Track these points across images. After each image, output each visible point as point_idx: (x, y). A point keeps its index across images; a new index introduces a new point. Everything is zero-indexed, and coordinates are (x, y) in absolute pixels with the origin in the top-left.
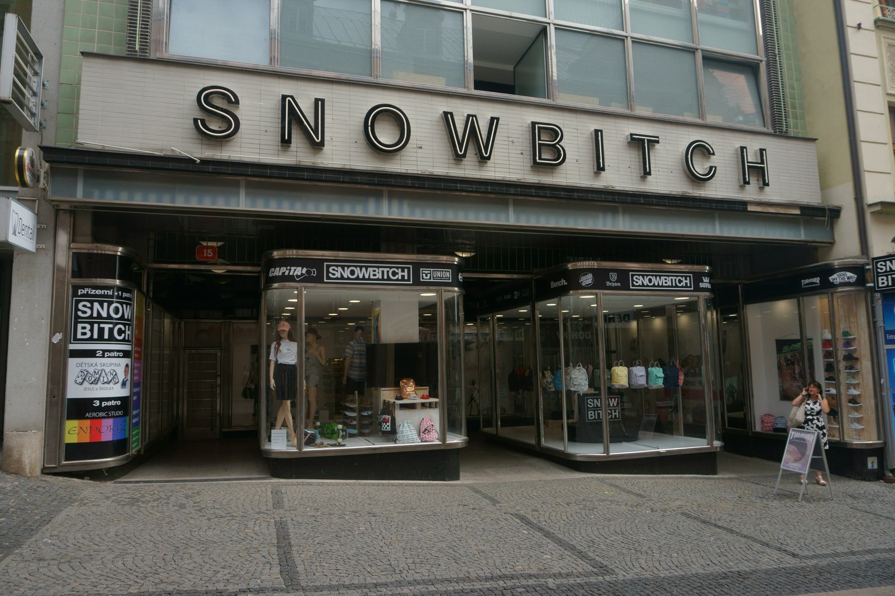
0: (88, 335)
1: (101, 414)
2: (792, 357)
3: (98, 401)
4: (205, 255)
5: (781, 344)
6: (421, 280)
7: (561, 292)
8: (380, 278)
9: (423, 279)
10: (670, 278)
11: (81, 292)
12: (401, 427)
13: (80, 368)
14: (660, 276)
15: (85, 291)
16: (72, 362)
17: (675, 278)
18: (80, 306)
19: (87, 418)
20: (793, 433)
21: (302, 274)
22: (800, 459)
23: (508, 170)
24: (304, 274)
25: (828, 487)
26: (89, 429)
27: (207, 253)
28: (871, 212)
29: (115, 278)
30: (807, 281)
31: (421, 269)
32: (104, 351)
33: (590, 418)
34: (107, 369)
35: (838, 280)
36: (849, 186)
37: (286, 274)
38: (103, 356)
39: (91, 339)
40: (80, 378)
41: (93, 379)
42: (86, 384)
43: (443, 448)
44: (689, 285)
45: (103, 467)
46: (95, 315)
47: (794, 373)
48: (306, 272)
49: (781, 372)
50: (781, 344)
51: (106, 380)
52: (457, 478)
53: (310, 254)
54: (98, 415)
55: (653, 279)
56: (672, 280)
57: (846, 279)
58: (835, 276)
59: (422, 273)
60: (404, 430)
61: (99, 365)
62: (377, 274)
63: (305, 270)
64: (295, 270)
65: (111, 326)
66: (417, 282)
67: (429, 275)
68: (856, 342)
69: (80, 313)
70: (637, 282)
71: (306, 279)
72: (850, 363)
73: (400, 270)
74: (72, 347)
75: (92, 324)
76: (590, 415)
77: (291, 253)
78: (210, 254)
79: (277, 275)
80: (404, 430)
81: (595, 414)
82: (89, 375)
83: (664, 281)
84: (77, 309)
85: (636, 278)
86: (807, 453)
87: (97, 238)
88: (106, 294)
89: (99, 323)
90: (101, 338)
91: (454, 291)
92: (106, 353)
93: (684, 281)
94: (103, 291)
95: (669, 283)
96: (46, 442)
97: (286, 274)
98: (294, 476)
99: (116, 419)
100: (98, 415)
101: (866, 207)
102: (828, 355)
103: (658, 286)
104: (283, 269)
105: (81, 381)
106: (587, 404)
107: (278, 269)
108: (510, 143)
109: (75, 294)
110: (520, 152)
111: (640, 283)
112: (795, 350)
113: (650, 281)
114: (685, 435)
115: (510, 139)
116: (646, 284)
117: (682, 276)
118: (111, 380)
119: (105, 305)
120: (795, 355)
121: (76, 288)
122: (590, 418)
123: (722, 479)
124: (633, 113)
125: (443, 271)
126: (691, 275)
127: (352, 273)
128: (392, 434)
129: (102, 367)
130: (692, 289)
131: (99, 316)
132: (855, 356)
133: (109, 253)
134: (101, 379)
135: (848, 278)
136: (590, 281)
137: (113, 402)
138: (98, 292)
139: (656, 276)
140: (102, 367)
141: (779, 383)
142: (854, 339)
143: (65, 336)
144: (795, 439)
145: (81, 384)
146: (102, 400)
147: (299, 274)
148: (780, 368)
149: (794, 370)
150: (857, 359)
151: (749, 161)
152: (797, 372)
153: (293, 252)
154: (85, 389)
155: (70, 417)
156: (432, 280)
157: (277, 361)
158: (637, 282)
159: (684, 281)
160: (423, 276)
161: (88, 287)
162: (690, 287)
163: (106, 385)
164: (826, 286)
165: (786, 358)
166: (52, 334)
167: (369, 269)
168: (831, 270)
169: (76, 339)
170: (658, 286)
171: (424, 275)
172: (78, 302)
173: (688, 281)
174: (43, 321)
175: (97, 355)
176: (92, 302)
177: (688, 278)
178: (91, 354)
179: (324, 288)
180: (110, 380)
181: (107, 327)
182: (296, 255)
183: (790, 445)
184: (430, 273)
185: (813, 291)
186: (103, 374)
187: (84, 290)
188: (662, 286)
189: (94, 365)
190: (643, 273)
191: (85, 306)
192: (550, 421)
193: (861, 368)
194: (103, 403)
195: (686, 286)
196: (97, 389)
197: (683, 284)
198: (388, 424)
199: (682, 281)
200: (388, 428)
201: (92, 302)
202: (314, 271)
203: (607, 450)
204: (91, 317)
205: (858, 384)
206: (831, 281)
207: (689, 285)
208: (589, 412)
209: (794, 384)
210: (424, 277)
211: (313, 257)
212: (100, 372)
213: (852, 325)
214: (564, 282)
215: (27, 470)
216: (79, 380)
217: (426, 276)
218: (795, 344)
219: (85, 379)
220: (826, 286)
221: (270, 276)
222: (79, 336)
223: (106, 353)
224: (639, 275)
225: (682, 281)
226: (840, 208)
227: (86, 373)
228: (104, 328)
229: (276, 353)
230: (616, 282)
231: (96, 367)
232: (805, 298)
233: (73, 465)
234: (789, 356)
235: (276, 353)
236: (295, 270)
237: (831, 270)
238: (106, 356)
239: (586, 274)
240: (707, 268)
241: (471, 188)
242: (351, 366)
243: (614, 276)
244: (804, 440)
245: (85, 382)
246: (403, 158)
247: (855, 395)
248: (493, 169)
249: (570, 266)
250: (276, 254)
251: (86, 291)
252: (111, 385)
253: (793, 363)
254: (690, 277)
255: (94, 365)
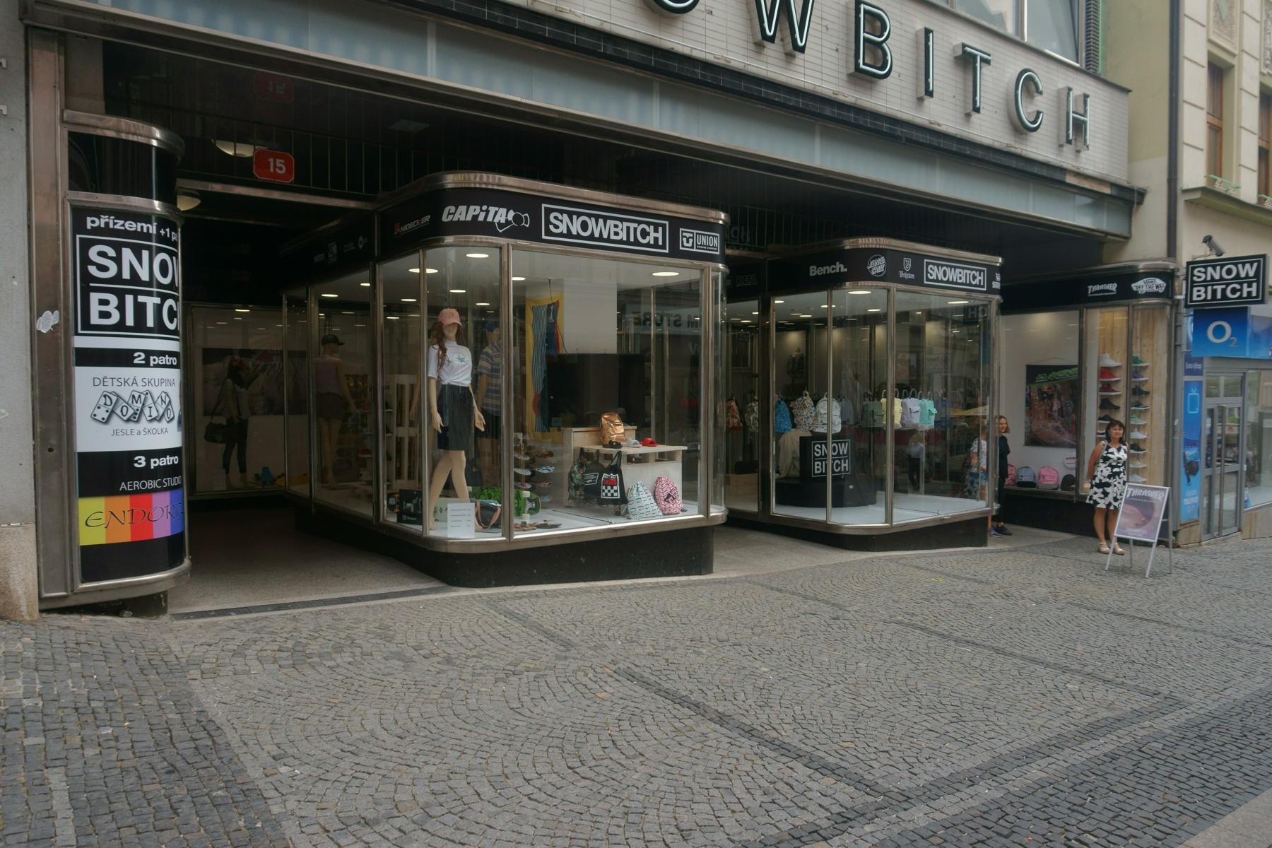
0: (115, 318)
1: (151, 484)
2: (1049, 388)
3: (143, 458)
4: (272, 170)
5: (1033, 372)
6: (681, 248)
7: (831, 283)
8: (625, 239)
9: (683, 246)
10: (626, 224)
11: (93, 222)
12: (635, 492)
13: (102, 389)
14: (605, 219)
15: (102, 221)
16: (84, 376)
17: (636, 225)
18: (93, 253)
19: (124, 493)
20: (1130, 490)
21: (508, 222)
22: (1144, 523)
23: (819, 75)
24: (510, 222)
25: (1127, 557)
26: (128, 514)
27: (275, 167)
28: (1186, 201)
29: (151, 197)
30: (1097, 288)
31: (681, 229)
32: (149, 353)
33: (816, 472)
34: (156, 392)
35: (1144, 288)
36: (1163, 162)
37: (481, 218)
38: (147, 365)
39: (120, 327)
40: (103, 409)
41: (131, 412)
42: (116, 422)
43: (704, 524)
44: (660, 243)
45: (159, 590)
46: (126, 275)
47: (1051, 410)
48: (514, 218)
49: (1030, 409)
50: (1033, 372)
51: (154, 414)
52: (710, 571)
53: (661, 208)
54: (144, 485)
55: (591, 223)
56: (628, 228)
57: (1155, 288)
58: (1141, 283)
59: (683, 237)
60: (641, 496)
61: (140, 383)
62: (620, 232)
63: (512, 214)
64: (496, 212)
65: (1224, 286)
66: (675, 252)
67: (691, 240)
68: (1148, 371)
69: (93, 270)
70: (556, 227)
71: (514, 231)
72: (1137, 398)
73: (652, 227)
74: (81, 342)
75: (121, 295)
76: (816, 467)
77: (478, 179)
78: (281, 169)
79: (462, 219)
80: (641, 496)
81: (822, 467)
82: (122, 403)
83: (613, 230)
84: (86, 261)
85: (556, 218)
86: (1156, 515)
87: (116, 104)
88: (145, 230)
89: (1213, 285)
90: (140, 327)
91: (718, 270)
92: (152, 358)
93: (653, 235)
94: (139, 225)
95: (623, 236)
96: (42, 546)
97: (481, 218)
98: (493, 583)
99: (174, 492)
100: (144, 485)
101: (1179, 192)
102: (1106, 387)
103: (601, 239)
104: (475, 210)
105: (106, 415)
106: (814, 451)
107: (463, 208)
108: (824, 29)
109: (79, 226)
110: (834, 47)
111: (934, 277)
112: (1055, 380)
113: (584, 226)
114: (928, 492)
115: (825, 23)
116: (574, 233)
117: (649, 224)
118: (163, 415)
119: (1218, 268)
120: (1055, 386)
121: (80, 213)
122: (816, 472)
123: (992, 552)
124: (953, 10)
125: (709, 236)
126: (667, 223)
127: (584, 226)
128: (620, 505)
129: (147, 388)
130: (667, 251)
131: (1213, 279)
132: (1144, 389)
133: (135, 138)
134: (146, 411)
135: (1157, 287)
136: (881, 269)
137: (168, 457)
138: (130, 226)
139: (597, 217)
140: (147, 388)
141: (1026, 423)
142: (1147, 367)
143: (65, 319)
144: (1135, 497)
145: (106, 421)
146: (150, 454)
147: (503, 221)
148: (1029, 402)
149: (1052, 406)
150: (1147, 393)
151: (866, 61)
152: (1055, 408)
153: (481, 178)
154: (116, 432)
155: (87, 492)
156: (695, 250)
157: (439, 381)
158: (556, 227)
159: (653, 235)
160: (682, 242)
161: (109, 212)
162: (663, 247)
163: (155, 425)
164: (1126, 294)
165: (1039, 389)
166: (36, 312)
167: (609, 222)
168: (1135, 275)
169: (87, 325)
170: (601, 239)
171: (685, 240)
172: (86, 245)
173: (660, 235)
174: (15, 283)
175: (136, 361)
176: (118, 247)
177: (660, 229)
178: (123, 358)
179: (543, 251)
180: (161, 413)
181: (1219, 288)
182: (480, 184)
183: (1127, 506)
184: (693, 238)
185: (1104, 300)
186: (150, 401)
187: (99, 218)
188: (609, 240)
189: (130, 382)
190: (573, 207)
191: (102, 254)
192: (733, 477)
193: (1151, 404)
194: (152, 460)
195: (656, 245)
196: (139, 433)
197: (650, 239)
198: (615, 488)
199: (648, 234)
200: (616, 494)
201: (118, 247)
202: (526, 217)
203: (889, 517)
204: (118, 278)
205: (1144, 426)
206: (1135, 289)
207: (660, 243)
208: (816, 463)
209: (1050, 425)
210: (685, 244)
211: (505, 189)
212: (143, 397)
213: (1145, 349)
214: (840, 268)
215: (24, 609)
216: (102, 414)
217: (688, 242)
218: (1057, 371)
219: (113, 412)
220: (1126, 294)
221: (444, 219)
222: (95, 319)
223: (152, 358)
224: (562, 212)
225: (648, 234)
226: (1145, 190)
227: (114, 399)
228: (144, 305)
229: (440, 365)
230: (910, 272)
231: (135, 387)
232: (1089, 311)
233: (101, 590)
234: (1045, 388)
235: (440, 365)
236: (496, 212)
237: (1135, 275)
238: (152, 363)
239: (877, 258)
240: (1000, 260)
241: (776, 96)
242: (488, 391)
243: (908, 263)
244: (1148, 498)
245: (115, 419)
246: (687, 27)
247: (1138, 440)
248: (801, 70)
249: (848, 244)
250: (452, 180)
251: (103, 221)
252: (164, 424)
253: (1051, 397)
254: (664, 226)
255: (130, 382)
